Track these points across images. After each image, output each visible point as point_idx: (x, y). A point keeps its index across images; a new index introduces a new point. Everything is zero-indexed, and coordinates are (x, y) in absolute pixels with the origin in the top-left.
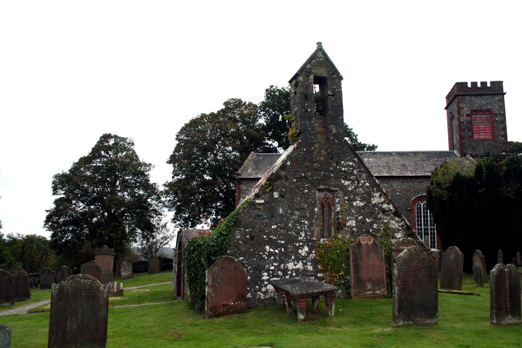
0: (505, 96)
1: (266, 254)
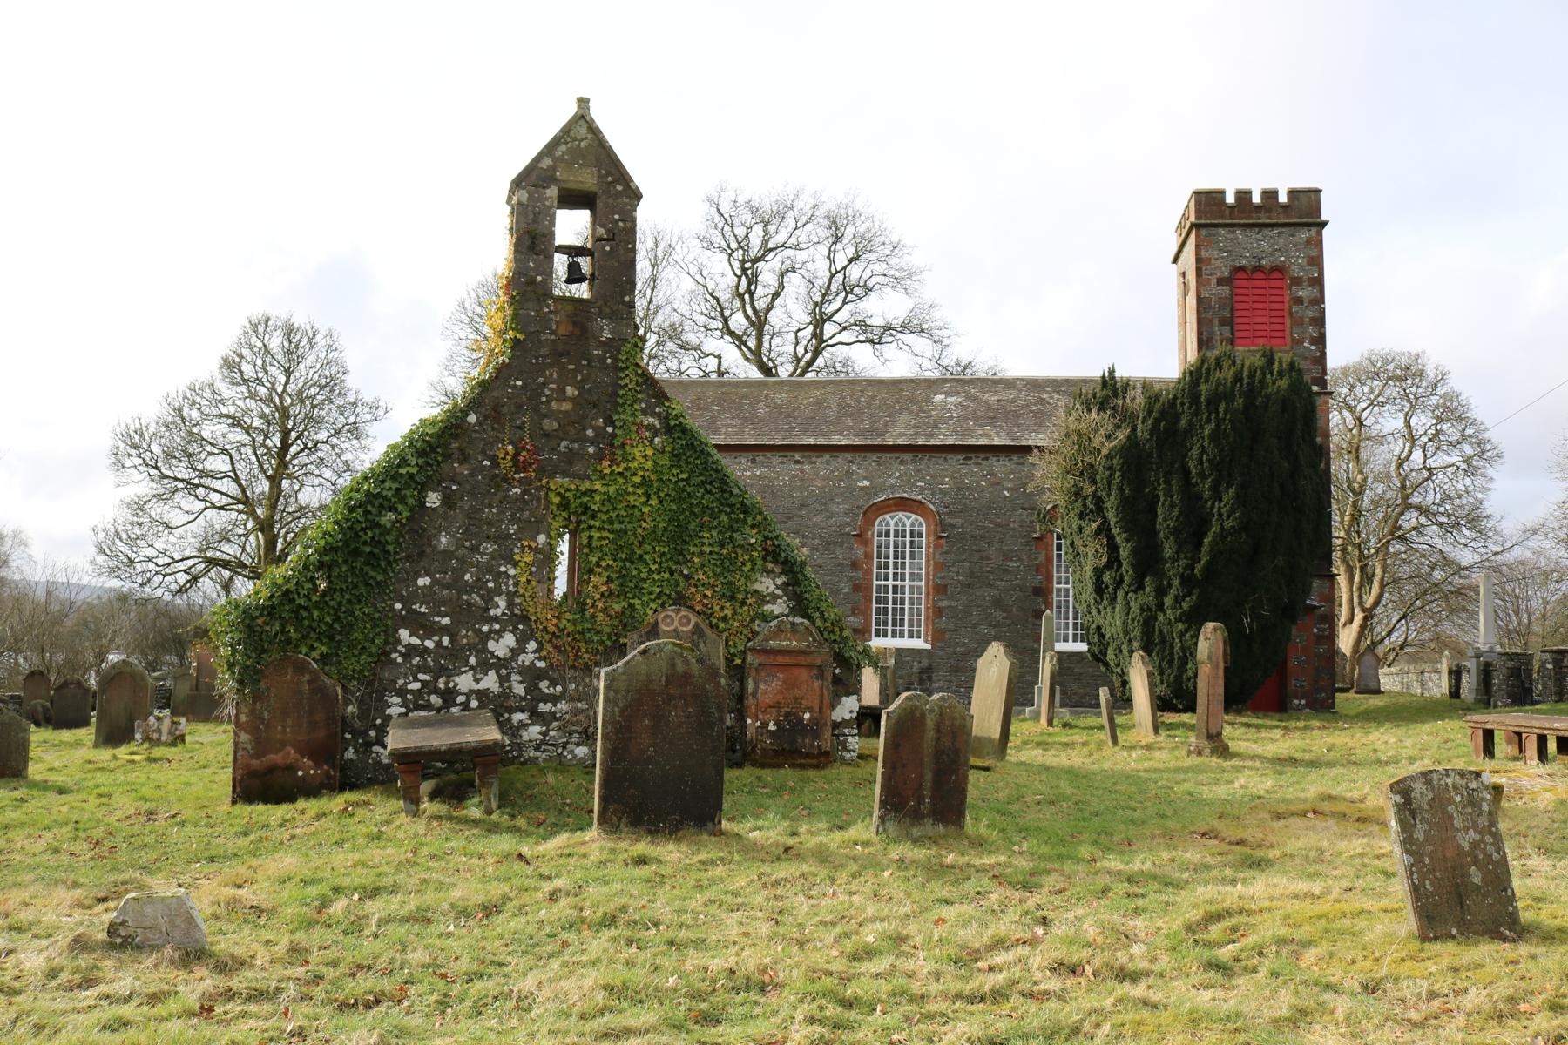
0: (1325, 231)
1: (400, 652)
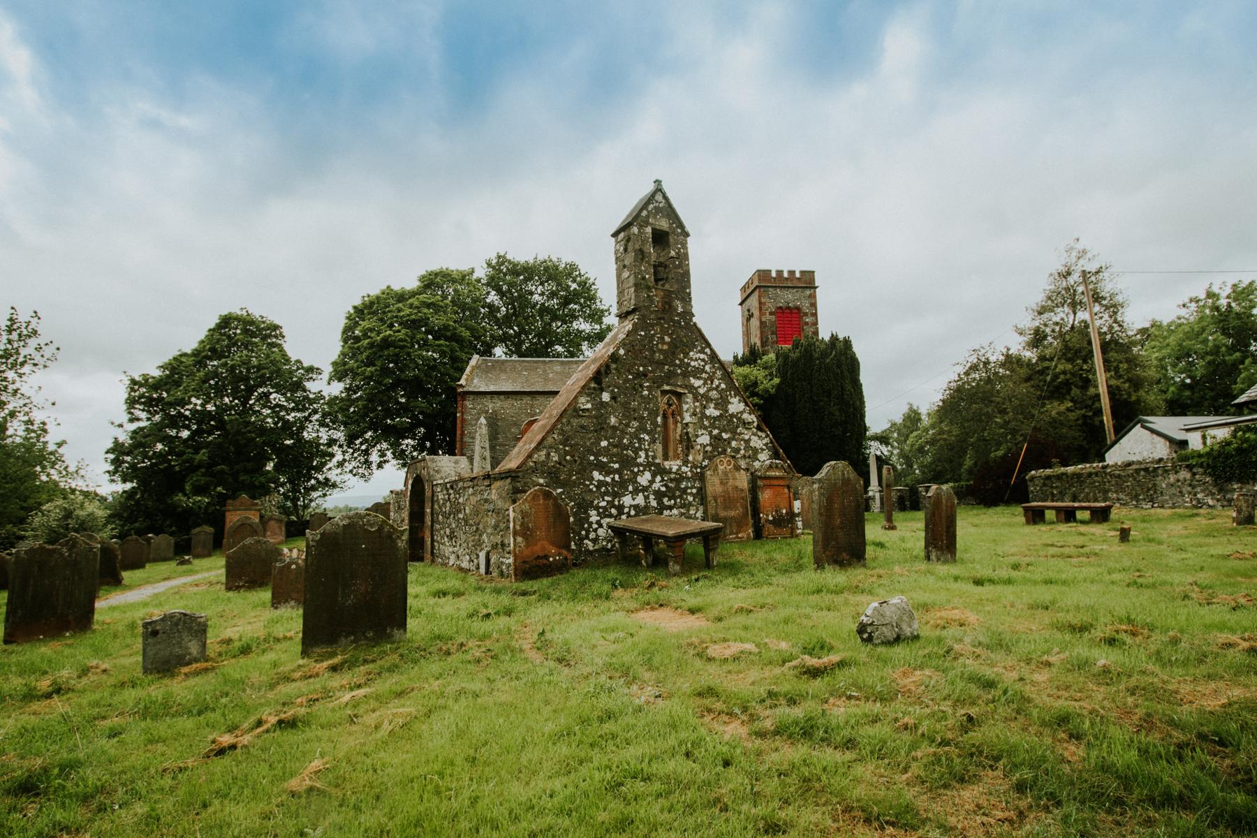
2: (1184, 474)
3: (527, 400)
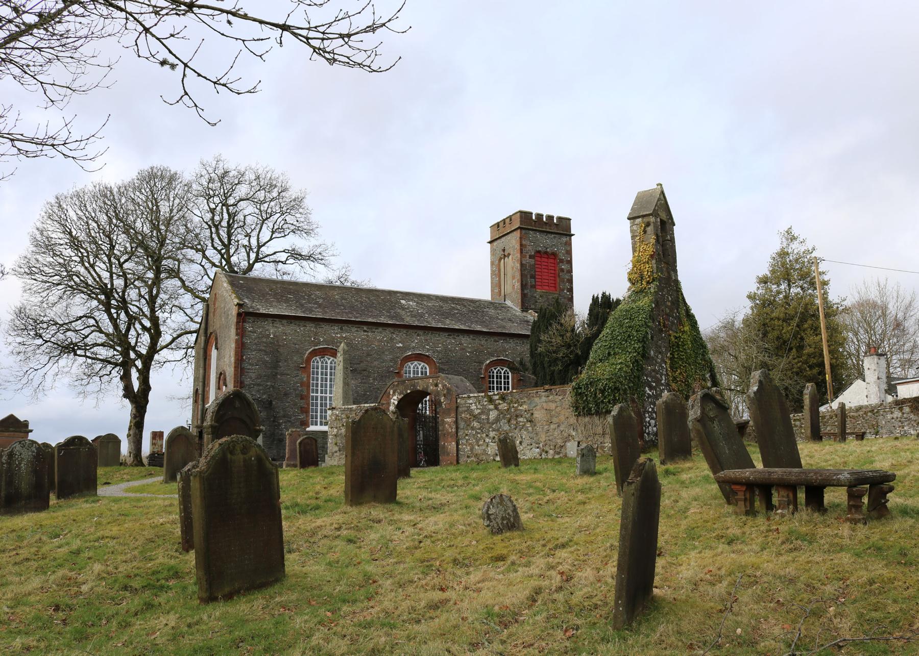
0: (572, 237)
2: (897, 414)
3: (310, 327)
